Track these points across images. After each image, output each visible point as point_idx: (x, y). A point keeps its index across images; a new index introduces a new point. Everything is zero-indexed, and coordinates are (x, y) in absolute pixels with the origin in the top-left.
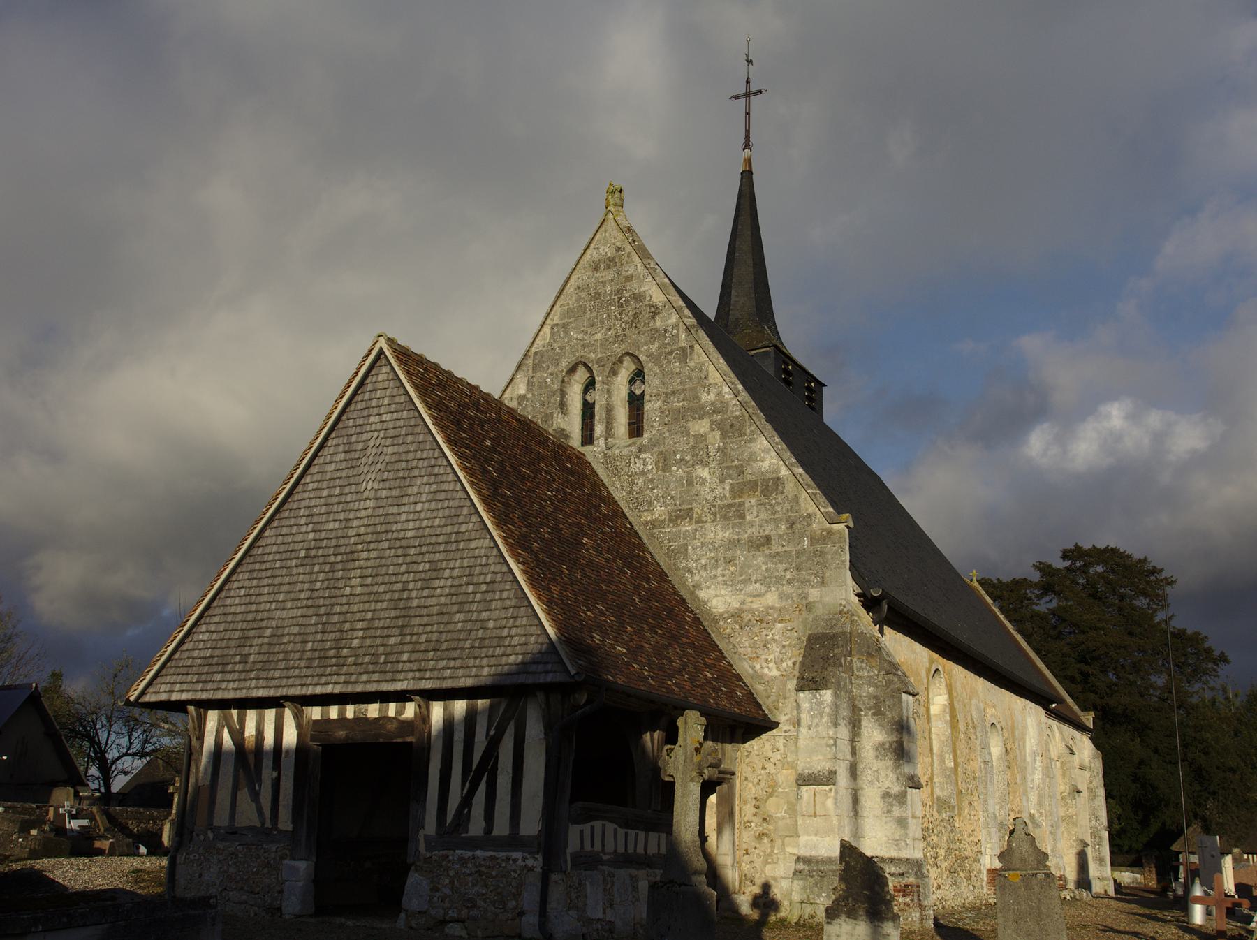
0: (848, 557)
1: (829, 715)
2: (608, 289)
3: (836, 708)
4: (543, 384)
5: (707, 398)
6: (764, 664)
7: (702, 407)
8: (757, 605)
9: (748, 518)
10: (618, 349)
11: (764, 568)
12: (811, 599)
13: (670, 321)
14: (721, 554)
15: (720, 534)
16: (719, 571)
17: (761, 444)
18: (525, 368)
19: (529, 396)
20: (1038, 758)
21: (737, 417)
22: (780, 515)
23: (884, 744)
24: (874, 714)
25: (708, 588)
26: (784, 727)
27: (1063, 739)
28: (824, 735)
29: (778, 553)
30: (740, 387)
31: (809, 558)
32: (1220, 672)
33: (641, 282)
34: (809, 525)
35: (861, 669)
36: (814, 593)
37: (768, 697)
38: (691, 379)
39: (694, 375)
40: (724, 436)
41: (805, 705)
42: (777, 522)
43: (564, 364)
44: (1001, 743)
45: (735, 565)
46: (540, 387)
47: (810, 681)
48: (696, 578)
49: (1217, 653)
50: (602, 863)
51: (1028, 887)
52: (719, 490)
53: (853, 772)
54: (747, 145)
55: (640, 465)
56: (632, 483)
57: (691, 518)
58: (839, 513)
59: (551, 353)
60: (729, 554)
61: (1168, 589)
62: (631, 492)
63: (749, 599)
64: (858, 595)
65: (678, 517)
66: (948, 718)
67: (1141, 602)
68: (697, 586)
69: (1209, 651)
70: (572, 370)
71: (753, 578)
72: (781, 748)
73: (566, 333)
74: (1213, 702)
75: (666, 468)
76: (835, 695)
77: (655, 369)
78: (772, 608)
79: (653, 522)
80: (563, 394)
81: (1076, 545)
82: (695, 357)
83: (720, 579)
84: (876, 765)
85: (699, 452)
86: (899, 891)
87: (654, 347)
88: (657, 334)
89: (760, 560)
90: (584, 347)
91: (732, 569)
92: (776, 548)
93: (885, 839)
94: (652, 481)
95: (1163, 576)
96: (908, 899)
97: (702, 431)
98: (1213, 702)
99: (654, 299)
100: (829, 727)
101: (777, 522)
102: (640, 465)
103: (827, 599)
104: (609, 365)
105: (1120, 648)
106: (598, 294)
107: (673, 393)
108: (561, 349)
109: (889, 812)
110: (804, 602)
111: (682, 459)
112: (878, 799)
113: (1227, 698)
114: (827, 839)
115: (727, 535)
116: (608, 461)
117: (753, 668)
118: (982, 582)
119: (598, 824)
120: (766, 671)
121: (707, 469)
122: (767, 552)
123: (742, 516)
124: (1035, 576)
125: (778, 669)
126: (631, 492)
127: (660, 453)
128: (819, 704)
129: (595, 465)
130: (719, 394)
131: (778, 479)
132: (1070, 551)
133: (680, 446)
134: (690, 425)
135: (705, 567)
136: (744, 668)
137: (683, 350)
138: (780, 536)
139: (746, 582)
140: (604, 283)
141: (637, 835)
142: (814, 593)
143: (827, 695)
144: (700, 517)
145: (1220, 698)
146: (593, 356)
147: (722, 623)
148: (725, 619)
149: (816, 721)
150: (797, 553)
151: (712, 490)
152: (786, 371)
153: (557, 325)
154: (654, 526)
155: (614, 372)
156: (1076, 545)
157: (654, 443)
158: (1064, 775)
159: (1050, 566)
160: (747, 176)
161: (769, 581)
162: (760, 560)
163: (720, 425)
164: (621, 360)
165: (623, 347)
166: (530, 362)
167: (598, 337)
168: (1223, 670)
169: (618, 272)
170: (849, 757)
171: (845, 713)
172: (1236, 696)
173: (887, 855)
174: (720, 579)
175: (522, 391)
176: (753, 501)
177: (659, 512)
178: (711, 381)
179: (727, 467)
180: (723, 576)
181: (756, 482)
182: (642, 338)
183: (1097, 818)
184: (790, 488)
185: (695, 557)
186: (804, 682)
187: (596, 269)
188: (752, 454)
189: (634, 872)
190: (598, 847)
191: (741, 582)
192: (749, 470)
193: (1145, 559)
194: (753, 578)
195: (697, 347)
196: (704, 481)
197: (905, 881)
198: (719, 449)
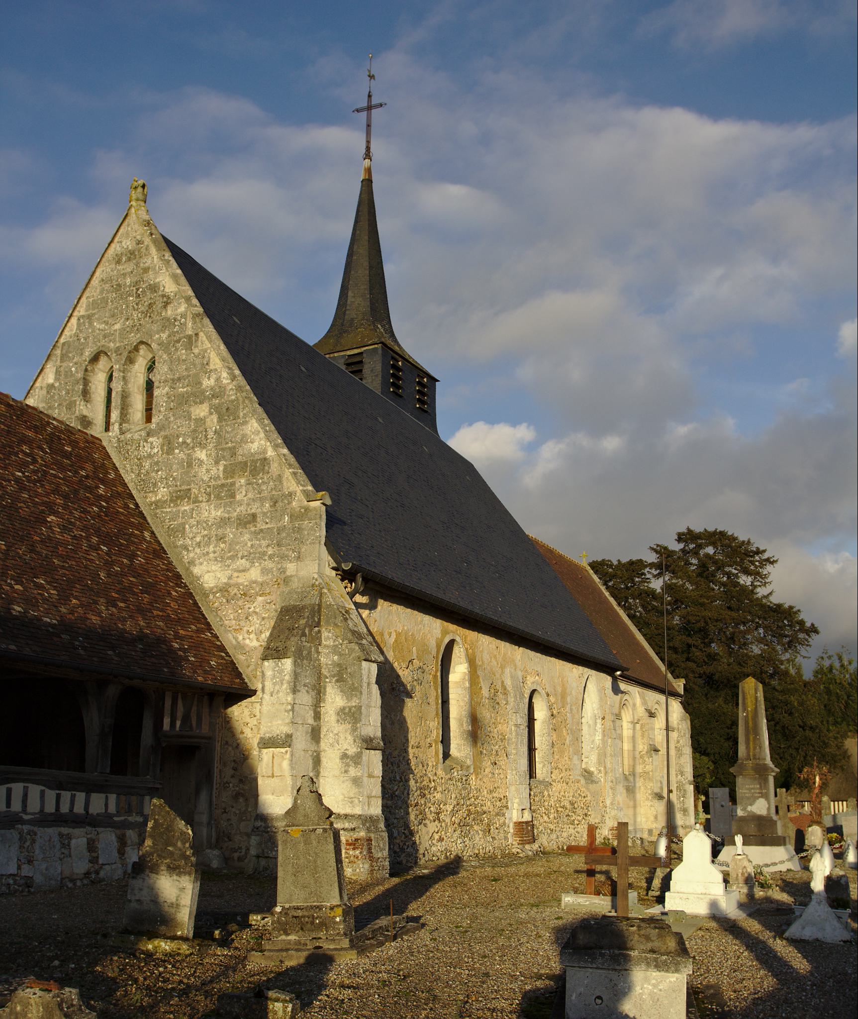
0: (324, 533)
1: (289, 683)
2: (128, 281)
3: (296, 675)
4: (69, 373)
5: (208, 383)
6: (246, 636)
7: (203, 392)
8: (243, 579)
9: (238, 497)
10: (134, 338)
11: (249, 544)
12: (288, 573)
13: (179, 311)
14: (213, 533)
15: (213, 512)
16: (211, 549)
17: (253, 425)
18: (54, 358)
19: (57, 384)
20: (599, 721)
21: (233, 401)
22: (265, 494)
23: (344, 708)
24: (337, 681)
25: (201, 564)
26: (259, 693)
27: (644, 703)
28: (284, 701)
29: (262, 530)
30: (237, 372)
31: (288, 535)
32: (811, 642)
33: (156, 273)
34: (289, 503)
35: (328, 638)
36: (291, 568)
37: (248, 666)
38: (194, 365)
39: (197, 361)
40: (220, 420)
41: (269, 673)
42: (262, 500)
43: (87, 354)
44: (545, 708)
45: (225, 542)
46: (66, 376)
47: (272, 652)
48: (191, 555)
49: (808, 624)
50: (23, 822)
51: (307, 842)
52: (214, 472)
53: (315, 734)
54: (368, 155)
55: (147, 449)
56: (140, 466)
57: (189, 498)
58: (317, 491)
59: (76, 344)
60: (220, 532)
61: (769, 568)
62: (139, 475)
63: (236, 574)
64: (333, 568)
65: (178, 498)
66: (467, 684)
67: (745, 580)
68: (192, 563)
69: (802, 623)
70: (95, 359)
71: (239, 556)
72: (258, 714)
73: (91, 324)
74: (831, 668)
75: (170, 451)
76: (295, 663)
77: (165, 356)
78: (255, 582)
79: (156, 503)
80: (86, 382)
81: (688, 529)
82: (200, 344)
83: (212, 555)
84: (338, 728)
85: (198, 436)
86: (350, 844)
87: (164, 336)
88: (168, 323)
89: (247, 537)
90: (105, 337)
91: (222, 546)
92: (261, 525)
93: (341, 797)
94: (157, 463)
95: (766, 556)
96: (357, 852)
97: (202, 414)
98: (831, 668)
99: (167, 290)
100: (288, 694)
101: (262, 500)
102: (147, 449)
103: (302, 573)
104: (125, 354)
105: (717, 621)
106: (119, 285)
107: (179, 379)
108: (85, 339)
109: (346, 772)
110: (283, 576)
111: (184, 442)
112: (338, 760)
113: (842, 666)
114: (282, 797)
115: (219, 514)
116: (122, 445)
117: (236, 639)
118: (590, 565)
119: (17, 788)
120: (247, 641)
121: (204, 451)
122: (253, 529)
123: (233, 496)
124: (652, 558)
125: (258, 640)
126: (139, 475)
127: (166, 437)
128: (281, 671)
129: (109, 450)
130: (218, 379)
131: (265, 459)
132: (683, 534)
133: (183, 430)
134: (192, 409)
135: (199, 545)
136: (228, 639)
137: (189, 337)
138: (265, 514)
139: (233, 558)
140: (124, 275)
141: (73, 798)
142: (291, 568)
143: (288, 664)
144: (197, 497)
145: (837, 665)
146: (112, 345)
147: (211, 597)
148: (214, 593)
149: (277, 687)
150: (278, 530)
151: (208, 471)
152: (394, 367)
153: (83, 316)
154: (157, 507)
155: (130, 361)
156: (688, 529)
157: (161, 427)
158: (643, 736)
159: (666, 548)
160: (367, 184)
161: (254, 557)
162: (247, 537)
163: (217, 409)
164: (136, 349)
165: (138, 336)
166: (58, 352)
167: (117, 326)
168: (815, 639)
169: (137, 265)
170: (311, 721)
171: (308, 678)
172: (850, 663)
173: (342, 812)
174: (212, 555)
175: (51, 380)
176: (243, 481)
177: (163, 492)
178: (212, 367)
179: (223, 449)
180: (214, 552)
181: (246, 463)
182: (155, 327)
183: (682, 774)
184: (274, 468)
185: (191, 535)
186: (270, 652)
187: (118, 262)
188: (244, 436)
189: (65, 830)
190: (16, 806)
191: (229, 558)
192: (240, 452)
193: (749, 542)
194: (239, 556)
195: (201, 334)
196: (201, 462)
197: (356, 835)
198: (216, 432)
